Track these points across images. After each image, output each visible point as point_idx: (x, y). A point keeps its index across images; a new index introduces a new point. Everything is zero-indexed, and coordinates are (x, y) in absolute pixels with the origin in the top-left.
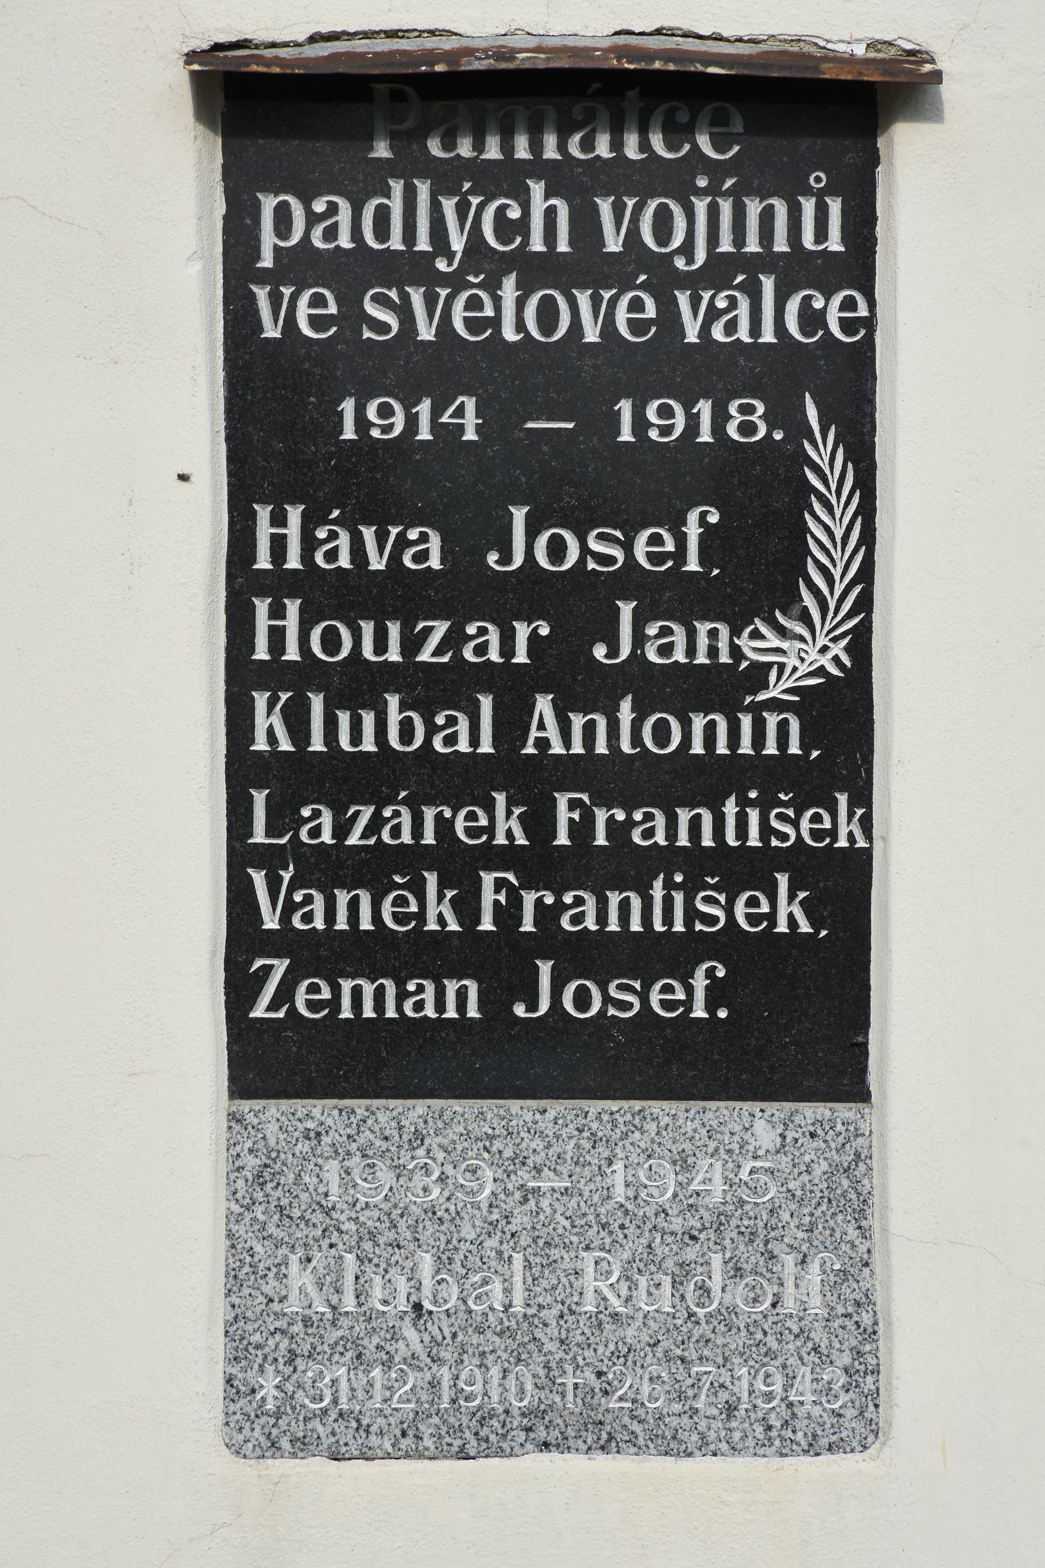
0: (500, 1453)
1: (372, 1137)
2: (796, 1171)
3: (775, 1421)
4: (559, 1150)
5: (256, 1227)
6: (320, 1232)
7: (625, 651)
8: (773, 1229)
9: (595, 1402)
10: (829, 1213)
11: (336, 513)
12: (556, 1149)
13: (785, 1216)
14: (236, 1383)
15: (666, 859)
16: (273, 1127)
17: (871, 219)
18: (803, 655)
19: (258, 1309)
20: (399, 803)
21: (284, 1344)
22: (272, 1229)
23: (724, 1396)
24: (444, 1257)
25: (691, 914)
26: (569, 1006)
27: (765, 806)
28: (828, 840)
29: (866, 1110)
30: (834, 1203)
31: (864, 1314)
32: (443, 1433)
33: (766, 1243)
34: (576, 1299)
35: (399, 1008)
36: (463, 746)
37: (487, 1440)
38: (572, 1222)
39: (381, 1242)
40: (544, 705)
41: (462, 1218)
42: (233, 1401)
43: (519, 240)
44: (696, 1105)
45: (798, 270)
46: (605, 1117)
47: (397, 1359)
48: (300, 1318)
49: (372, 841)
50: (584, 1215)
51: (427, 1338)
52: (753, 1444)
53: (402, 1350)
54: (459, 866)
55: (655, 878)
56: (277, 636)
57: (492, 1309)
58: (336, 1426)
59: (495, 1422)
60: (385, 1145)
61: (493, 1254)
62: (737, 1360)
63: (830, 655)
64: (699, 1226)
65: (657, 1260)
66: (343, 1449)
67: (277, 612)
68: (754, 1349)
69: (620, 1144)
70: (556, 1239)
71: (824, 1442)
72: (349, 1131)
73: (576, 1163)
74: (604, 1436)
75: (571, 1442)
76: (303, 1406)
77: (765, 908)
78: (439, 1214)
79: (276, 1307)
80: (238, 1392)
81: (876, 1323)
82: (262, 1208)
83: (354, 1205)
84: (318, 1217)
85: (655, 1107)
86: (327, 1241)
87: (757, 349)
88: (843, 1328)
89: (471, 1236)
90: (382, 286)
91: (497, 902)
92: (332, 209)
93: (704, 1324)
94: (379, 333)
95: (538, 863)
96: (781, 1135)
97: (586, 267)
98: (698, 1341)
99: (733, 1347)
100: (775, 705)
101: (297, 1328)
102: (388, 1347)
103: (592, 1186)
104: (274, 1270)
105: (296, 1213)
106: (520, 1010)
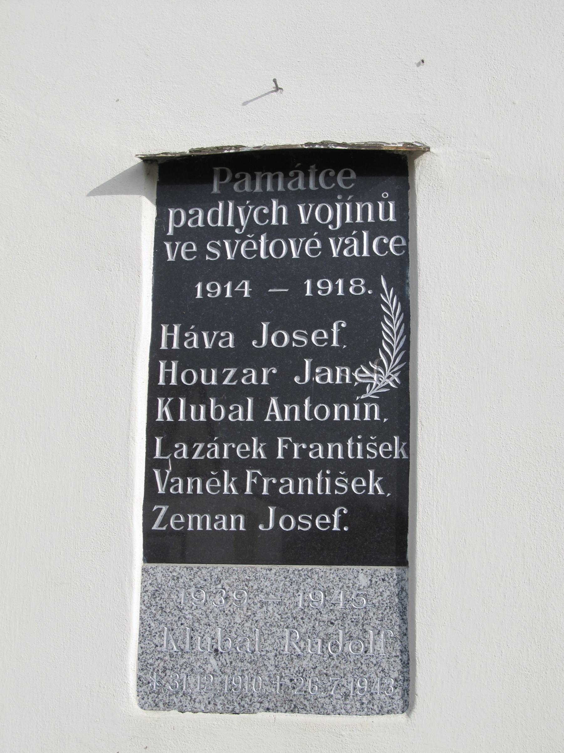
0: (249, 712)
1: (200, 579)
2: (376, 595)
3: (364, 700)
4: (276, 586)
5: (152, 616)
6: (177, 619)
7: (307, 378)
8: (366, 620)
9: (289, 692)
10: (390, 613)
11: (193, 327)
12: (275, 586)
13: (371, 614)
14: (142, 679)
15: (323, 464)
16: (160, 575)
17: (406, 209)
18: (380, 379)
19: (152, 649)
20: (215, 442)
21: (162, 664)
22: (158, 617)
23: (343, 690)
24: (228, 630)
25: (333, 487)
26: (281, 525)
27: (364, 443)
28: (391, 456)
29: (406, 569)
30: (392, 609)
31: (404, 656)
32: (226, 703)
33: (363, 625)
34: (282, 648)
35: (212, 526)
36: (240, 418)
37: (244, 707)
38: (281, 616)
39: (202, 623)
40: (274, 401)
41: (235, 614)
42: (141, 686)
43: (267, 221)
44: (334, 567)
45: (377, 228)
46: (296, 572)
47: (207, 672)
48: (168, 654)
49: (203, 458)
50: (287, 613)
51: (220, 663)
52: (355, 710)
53: (209, 669)
54: (238, 467)
55: (318, 472)
56: (168, 376)
57: (247, 652)
58: (182, 698)
59: (247, 699)
60: (205, 583)
61: (248, 629)
62: (349, 675)
63: (391, 379)
64: (335, 618)
65: (317, 632)
66: (185, 708)
67: (168, 366)
68: (357, 670)
69: (302, 584)
70: (275, 623)
71: (386, 710)
72: (190, 577)
73: (284, 592)
74: (293, 706)
75: (279, 708)
76: (169, 690)
77: (364, 484)
78: (226, 612)
79: (159, 648)
80: (143, 683)
81: (409, 660)
82: (154, 608)
83: (192, 608)
84: (177, 612)
85: (317, 568)
86: (180, 622)
87: (361, 259)
88: (395, 661)
89: (239, 621)
90: (214, 240)
91: (253, 482)
92: (197, 213)
93: (336, 660)
94: (212, 257)
95: (270, 466)
96: (370, 580)
97: (294, 230)
98: (333, 667)
99: (348, 669)
100: (369, 400)
101: (167, 658)
102: (204, 667)
103: (290, 601)
104: (159, 633)
105: (168, 610)
106: (261, 527)
